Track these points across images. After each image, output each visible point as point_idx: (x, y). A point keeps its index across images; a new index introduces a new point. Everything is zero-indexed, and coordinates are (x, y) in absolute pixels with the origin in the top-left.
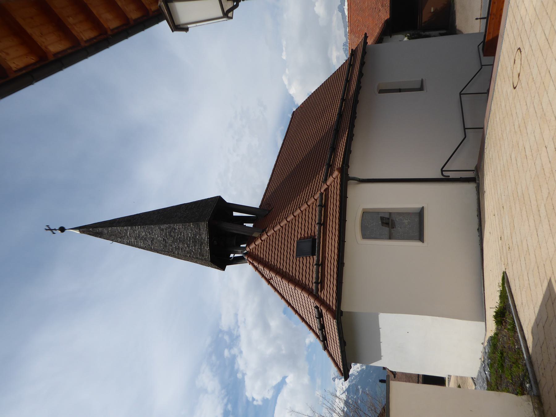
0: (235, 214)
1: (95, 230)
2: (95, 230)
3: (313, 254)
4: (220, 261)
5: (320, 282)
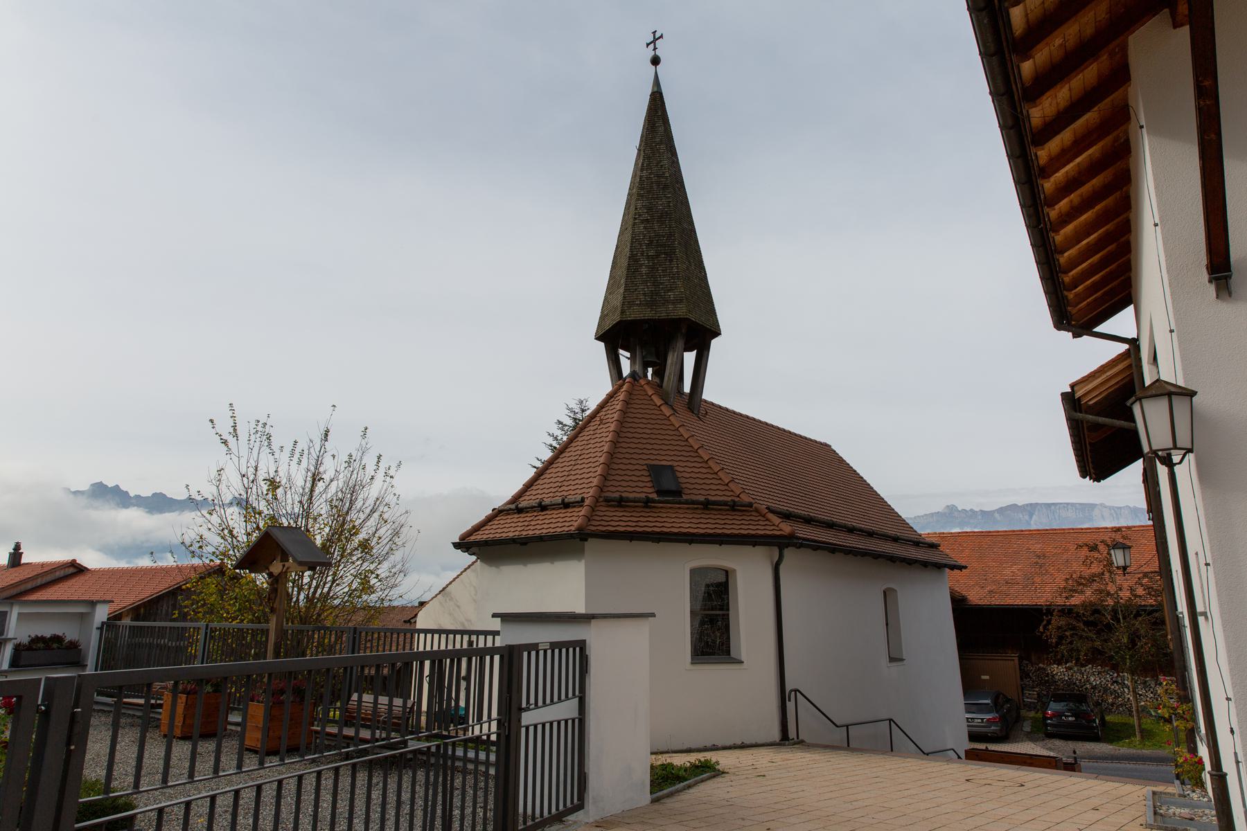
0: (690, 358)
1: (657, 104)
2: (657, 104)
3: (659, 492)
4: (614, 336)
5: (621, 503)
